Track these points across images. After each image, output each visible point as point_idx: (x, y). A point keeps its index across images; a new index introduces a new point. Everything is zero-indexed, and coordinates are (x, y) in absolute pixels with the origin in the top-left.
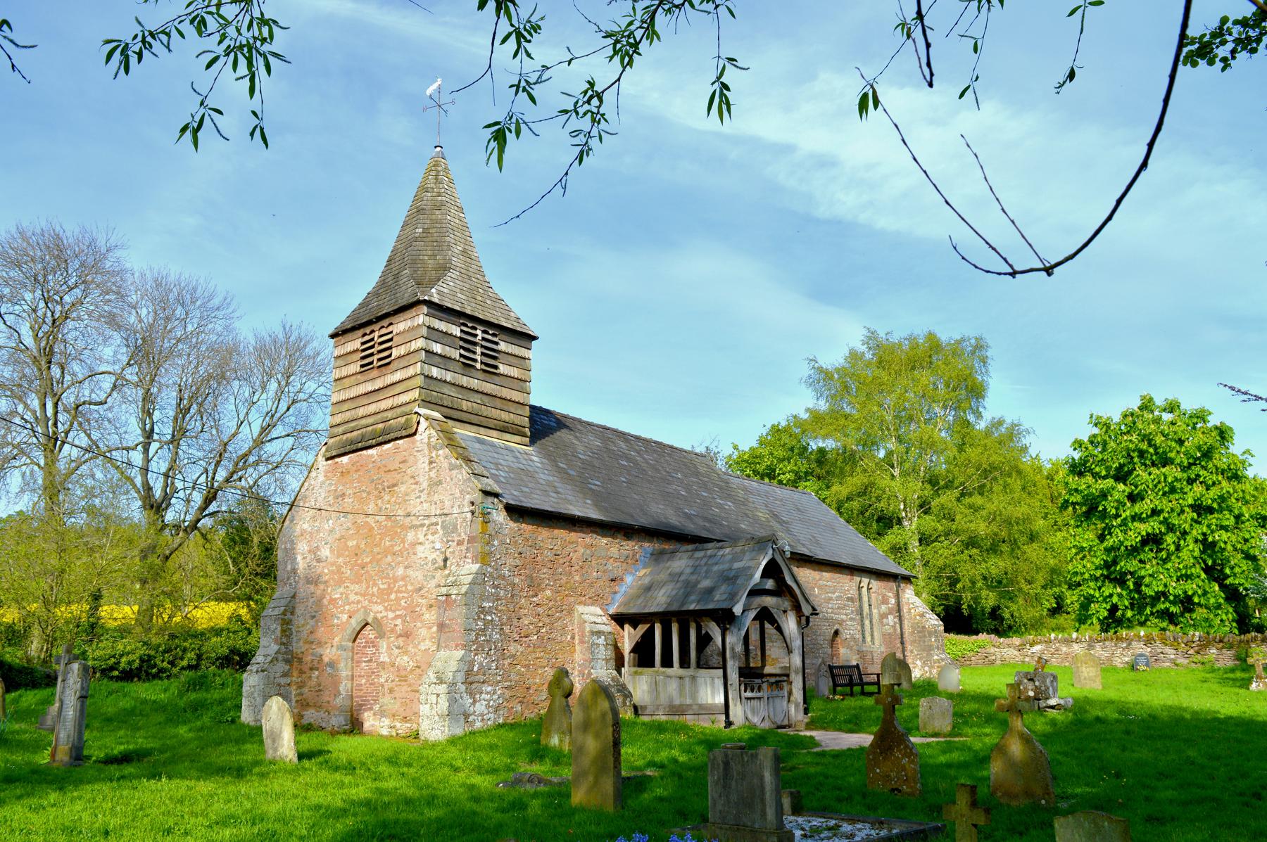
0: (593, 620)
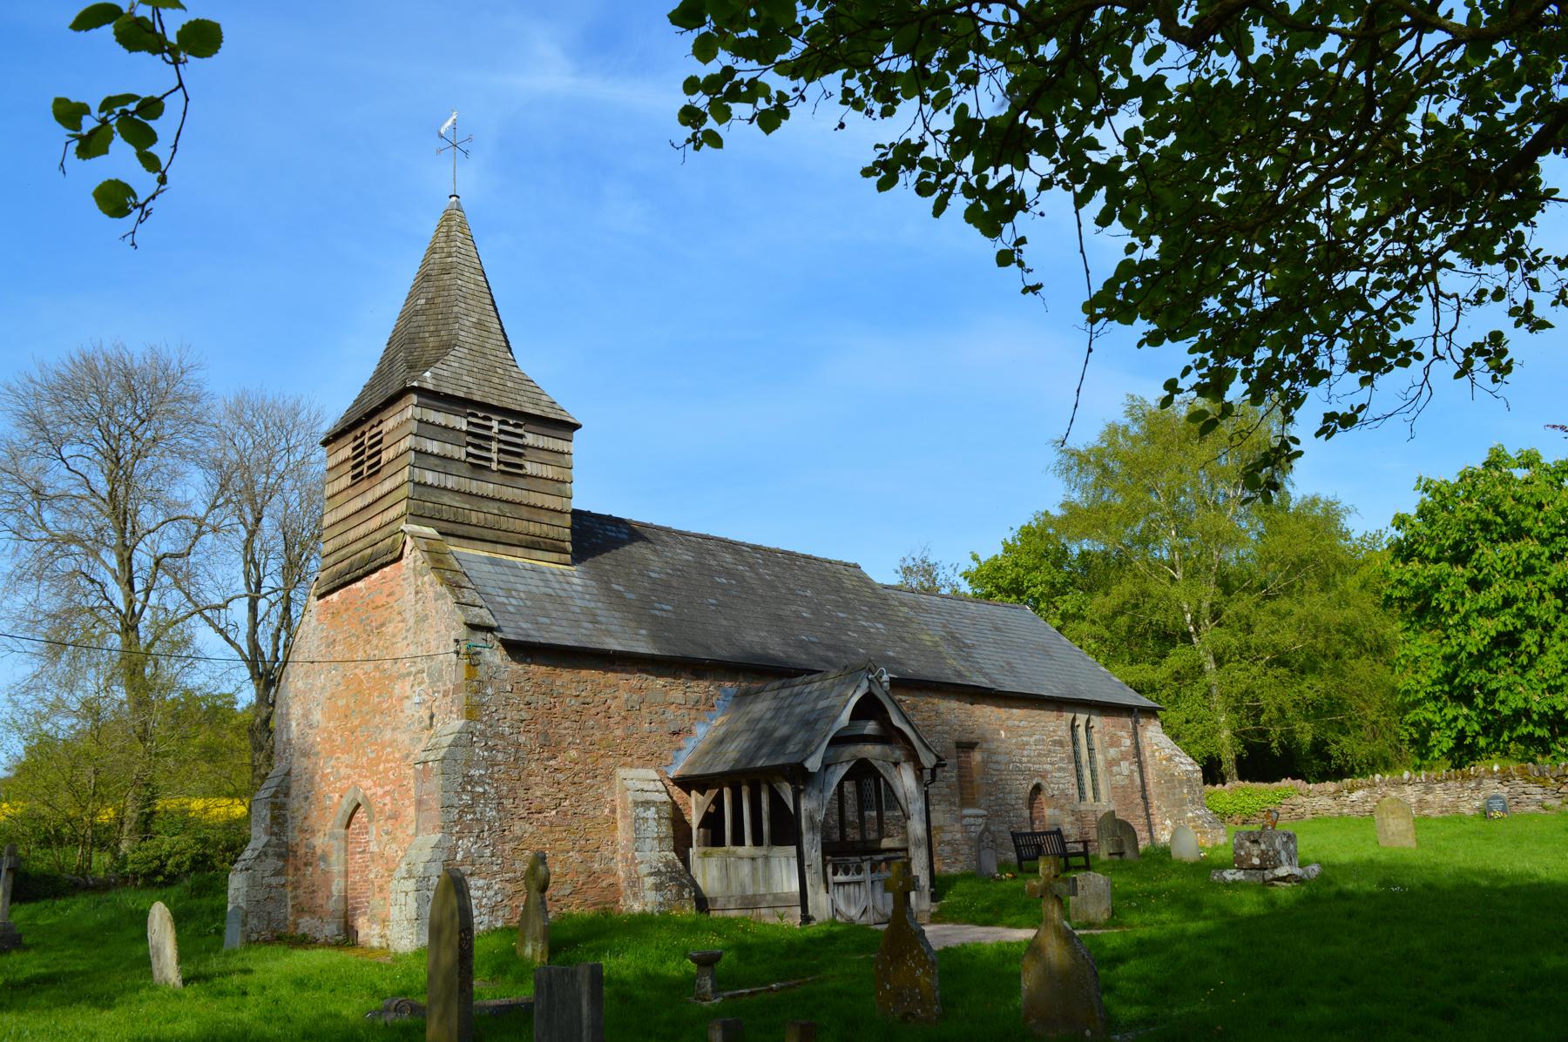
0: (640, 787)
